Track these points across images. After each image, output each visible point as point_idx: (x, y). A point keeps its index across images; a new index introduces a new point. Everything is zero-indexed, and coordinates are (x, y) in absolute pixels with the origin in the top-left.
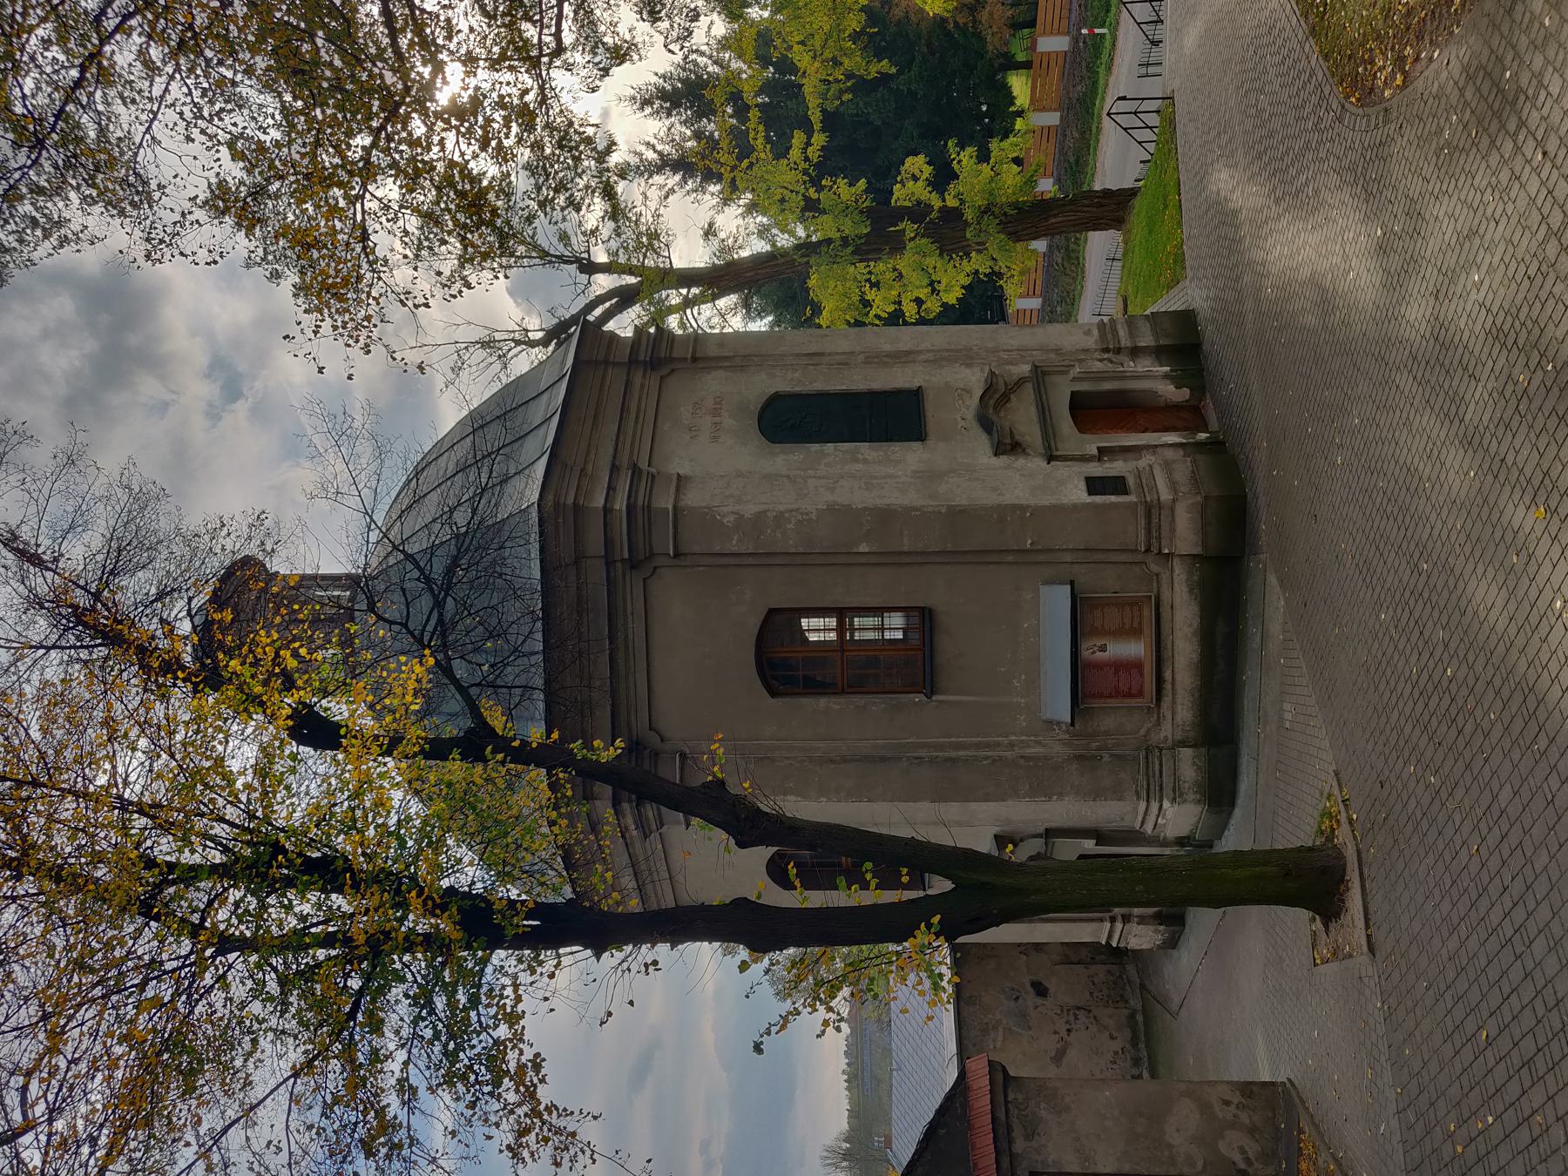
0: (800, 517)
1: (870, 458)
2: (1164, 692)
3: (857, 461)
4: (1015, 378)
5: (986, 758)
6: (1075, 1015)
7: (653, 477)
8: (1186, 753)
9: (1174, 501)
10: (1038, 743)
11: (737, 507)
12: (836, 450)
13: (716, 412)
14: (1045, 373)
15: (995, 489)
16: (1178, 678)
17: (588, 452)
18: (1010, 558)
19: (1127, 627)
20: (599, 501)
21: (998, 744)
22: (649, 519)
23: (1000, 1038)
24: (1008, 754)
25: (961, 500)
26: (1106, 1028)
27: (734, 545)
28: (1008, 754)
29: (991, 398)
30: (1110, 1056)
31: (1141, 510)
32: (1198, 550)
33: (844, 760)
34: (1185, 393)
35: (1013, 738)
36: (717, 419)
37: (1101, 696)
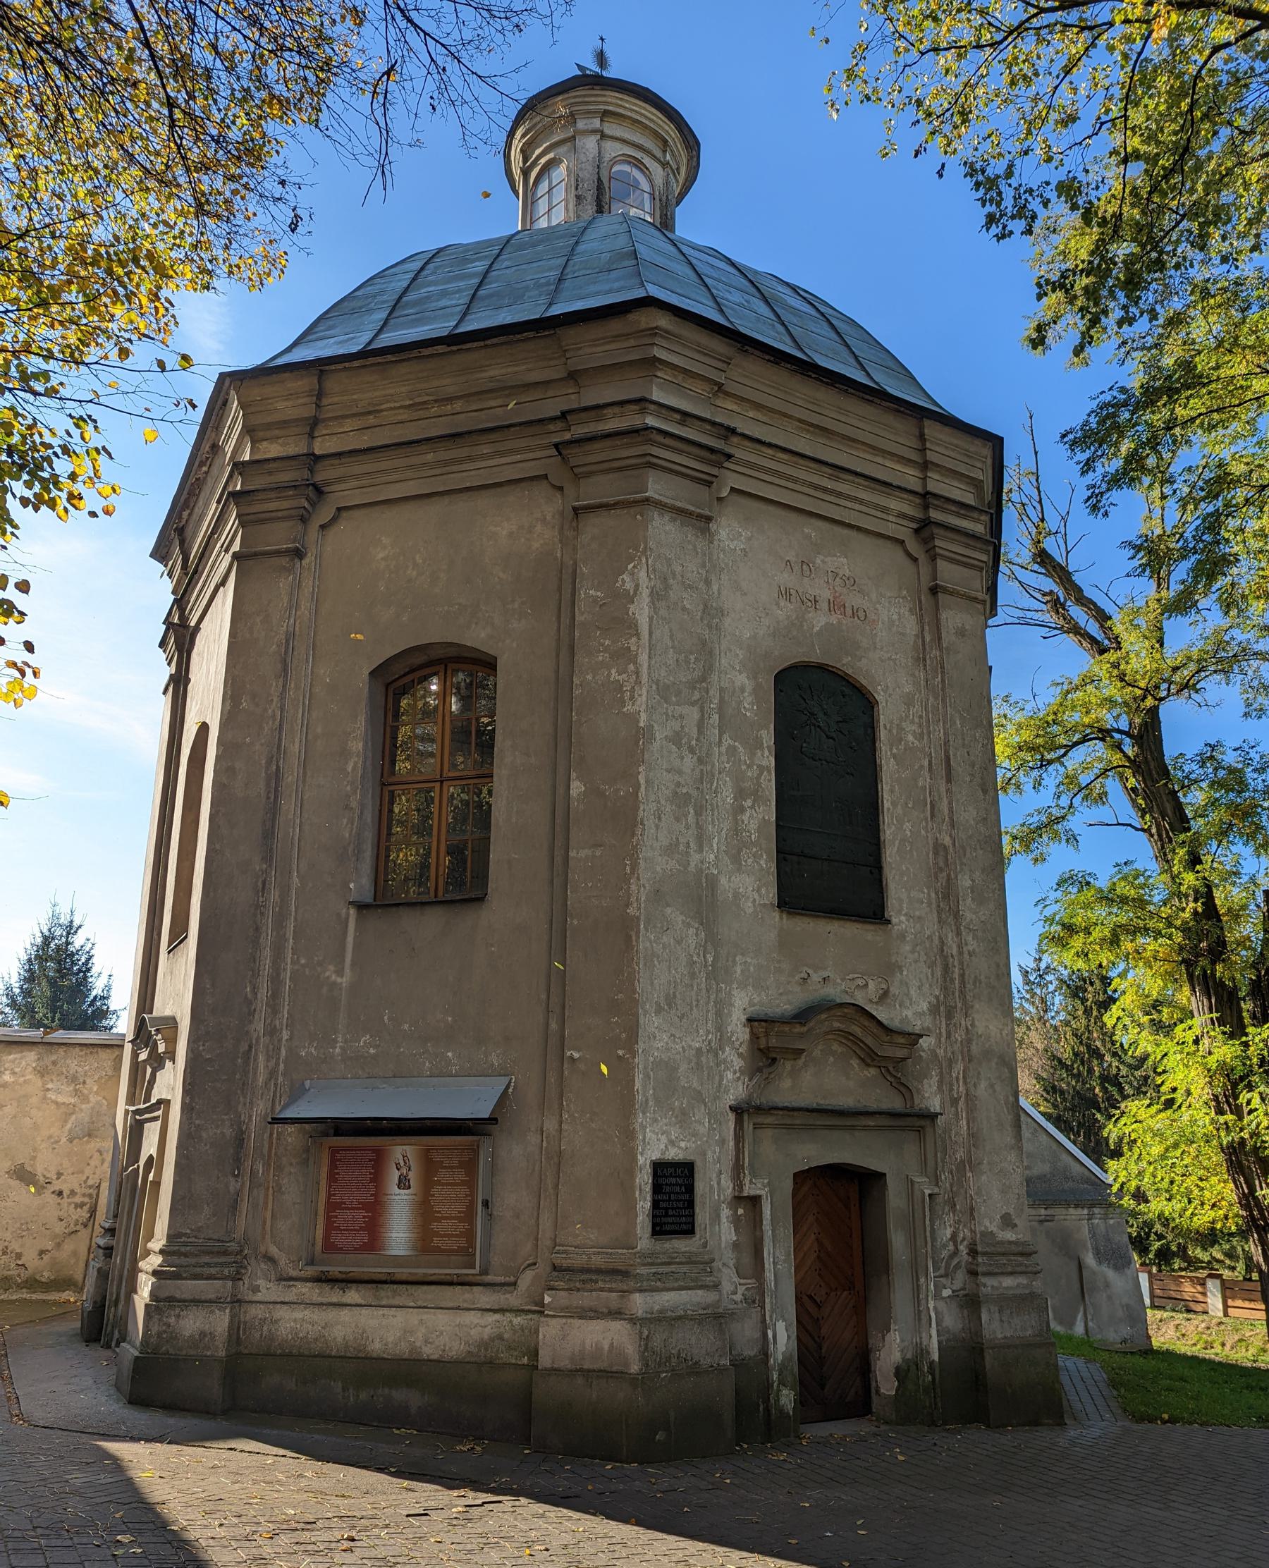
0: (627, 687)
1: (746, 817)
2: (326, 1287)
3: (740, 794)
4: (913, 1084)
5: (255, 991)
6: (82, 1205)
7: (709, 484)
8: (220, 1322)
10: (272, 1074)
12: (762, 769)
13: (836, 605)
14: (920, 1130)
16: (345, 1314)
17: (758, 406)
18: (554, 1026)
19: (434, 1226)
20: (657, 395)
21: (274, 1009)
22: (627, 468)
23: (61, 1099)
24: (258, 1026)
25: (646, 941)
26: (59, 1245)
27: (589, 592)
28: (259, 1026)
29: (864, 1027)
30: (15, 1246)
32: (545, 1360)
34: (886, 1385)
35: (285, 1035)
37: (332, 1178)
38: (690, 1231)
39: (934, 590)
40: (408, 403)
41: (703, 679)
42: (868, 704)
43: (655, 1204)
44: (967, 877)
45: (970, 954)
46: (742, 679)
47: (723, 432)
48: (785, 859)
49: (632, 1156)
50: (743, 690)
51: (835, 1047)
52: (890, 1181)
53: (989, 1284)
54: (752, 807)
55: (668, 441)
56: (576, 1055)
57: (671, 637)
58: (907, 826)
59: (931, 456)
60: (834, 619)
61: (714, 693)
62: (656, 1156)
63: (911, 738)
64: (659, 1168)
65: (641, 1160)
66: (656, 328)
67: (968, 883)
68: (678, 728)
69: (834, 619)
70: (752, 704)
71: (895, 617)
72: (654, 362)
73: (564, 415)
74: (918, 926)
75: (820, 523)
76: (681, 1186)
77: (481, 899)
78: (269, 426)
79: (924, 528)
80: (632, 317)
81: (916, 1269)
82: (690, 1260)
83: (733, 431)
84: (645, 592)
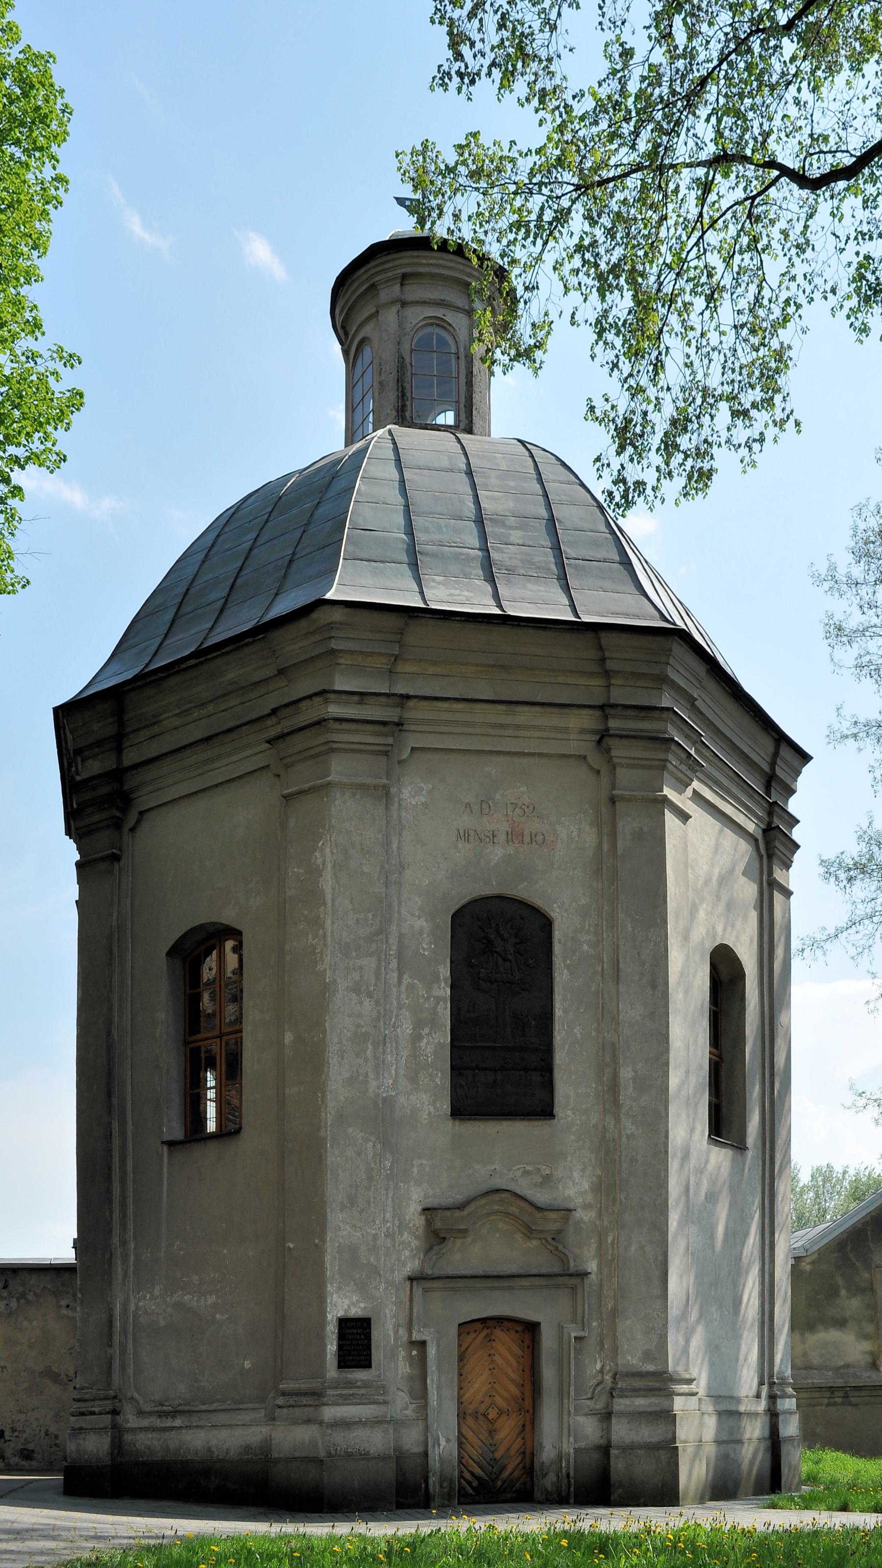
3: (418, 1024)
9: (321, 1423)
11: (329, 866)
12: (438, 999)
13: (515, 835)
14: (574, 1288)
15: (352, 1201)
24: (116, 1240)
25: (332, 1157)
30: (53, 1429)
31: (315, 1384)
33: (110, 1048)
35: (132, 1246)
36: (501, 838)
38: (368, 1365)
39: (613, 800)
40: (177, 711)
41: (379, 932)
42: (547, 924)
43: (340, 1347)
44: (629, 1069)
45: (628, 1137)
46: (422, 923)
47: (398, 700)
48: (460, 1074)
49: (323, 1313)
50: (421, 932)
51: (501, 1225)
52: (544, 1328)
53: (621, 1404)
54: (429, 1034)
55: (345, 726)
56: (291, 1246)
57: (351, 902)
58: (577, 1030)
59: (610, 665)
60: (511, 850)
61: (393, 941)
62: (341, 1314)
63: (585, 947)
64: (344, 1323)
65: (329, 1317)
66: (331, 623)
67: (630, 1074)
68: (358, 978)
69: (511, 850)
70: (430, 943)
71: (575, 834)
72: (333, 652)
73: (274, 712)
74: (583, 1117)
75: (501, 759)
76: (360, 1334)
77: (238, 1131)
78: (90, 746)
79: (603, 737)
80: (314, 615)
81: (562, 1393)
82: (366, 1385)
83: (408, 697)
84: (329, 866)
